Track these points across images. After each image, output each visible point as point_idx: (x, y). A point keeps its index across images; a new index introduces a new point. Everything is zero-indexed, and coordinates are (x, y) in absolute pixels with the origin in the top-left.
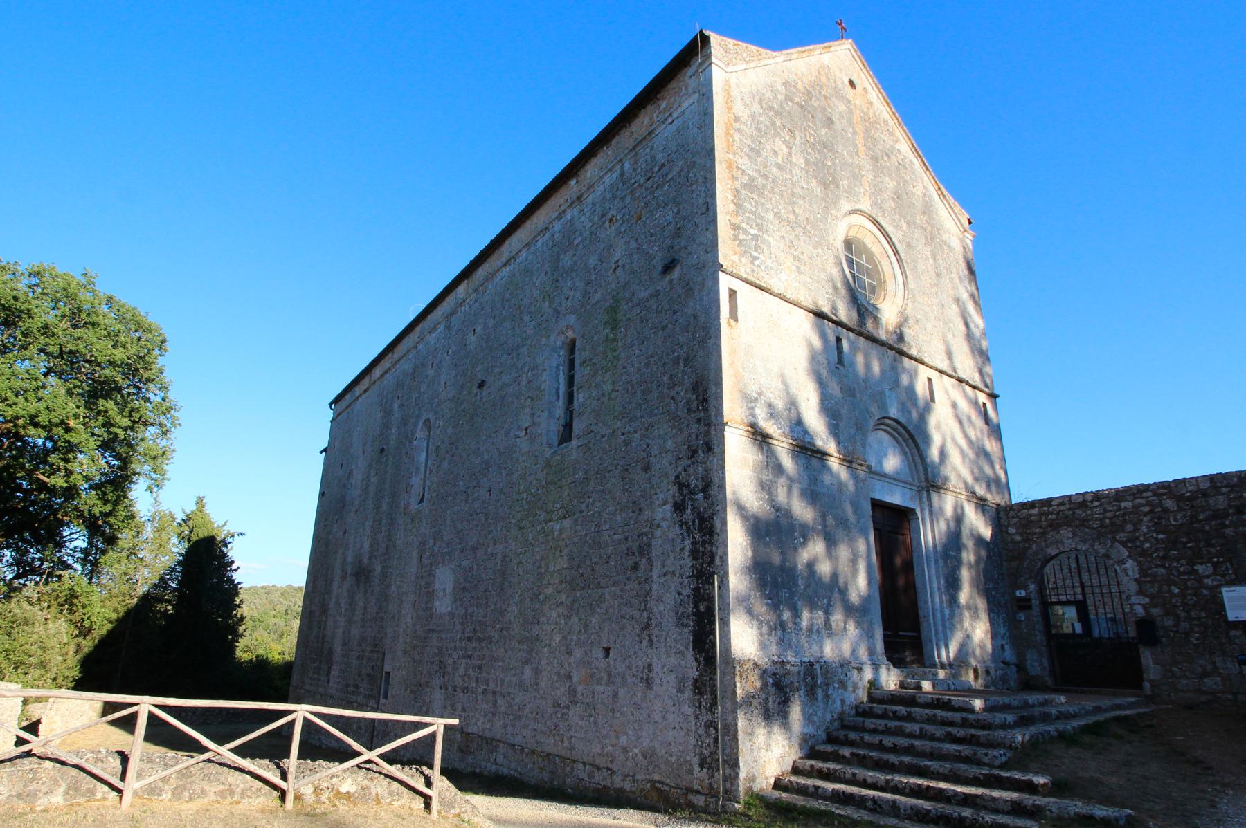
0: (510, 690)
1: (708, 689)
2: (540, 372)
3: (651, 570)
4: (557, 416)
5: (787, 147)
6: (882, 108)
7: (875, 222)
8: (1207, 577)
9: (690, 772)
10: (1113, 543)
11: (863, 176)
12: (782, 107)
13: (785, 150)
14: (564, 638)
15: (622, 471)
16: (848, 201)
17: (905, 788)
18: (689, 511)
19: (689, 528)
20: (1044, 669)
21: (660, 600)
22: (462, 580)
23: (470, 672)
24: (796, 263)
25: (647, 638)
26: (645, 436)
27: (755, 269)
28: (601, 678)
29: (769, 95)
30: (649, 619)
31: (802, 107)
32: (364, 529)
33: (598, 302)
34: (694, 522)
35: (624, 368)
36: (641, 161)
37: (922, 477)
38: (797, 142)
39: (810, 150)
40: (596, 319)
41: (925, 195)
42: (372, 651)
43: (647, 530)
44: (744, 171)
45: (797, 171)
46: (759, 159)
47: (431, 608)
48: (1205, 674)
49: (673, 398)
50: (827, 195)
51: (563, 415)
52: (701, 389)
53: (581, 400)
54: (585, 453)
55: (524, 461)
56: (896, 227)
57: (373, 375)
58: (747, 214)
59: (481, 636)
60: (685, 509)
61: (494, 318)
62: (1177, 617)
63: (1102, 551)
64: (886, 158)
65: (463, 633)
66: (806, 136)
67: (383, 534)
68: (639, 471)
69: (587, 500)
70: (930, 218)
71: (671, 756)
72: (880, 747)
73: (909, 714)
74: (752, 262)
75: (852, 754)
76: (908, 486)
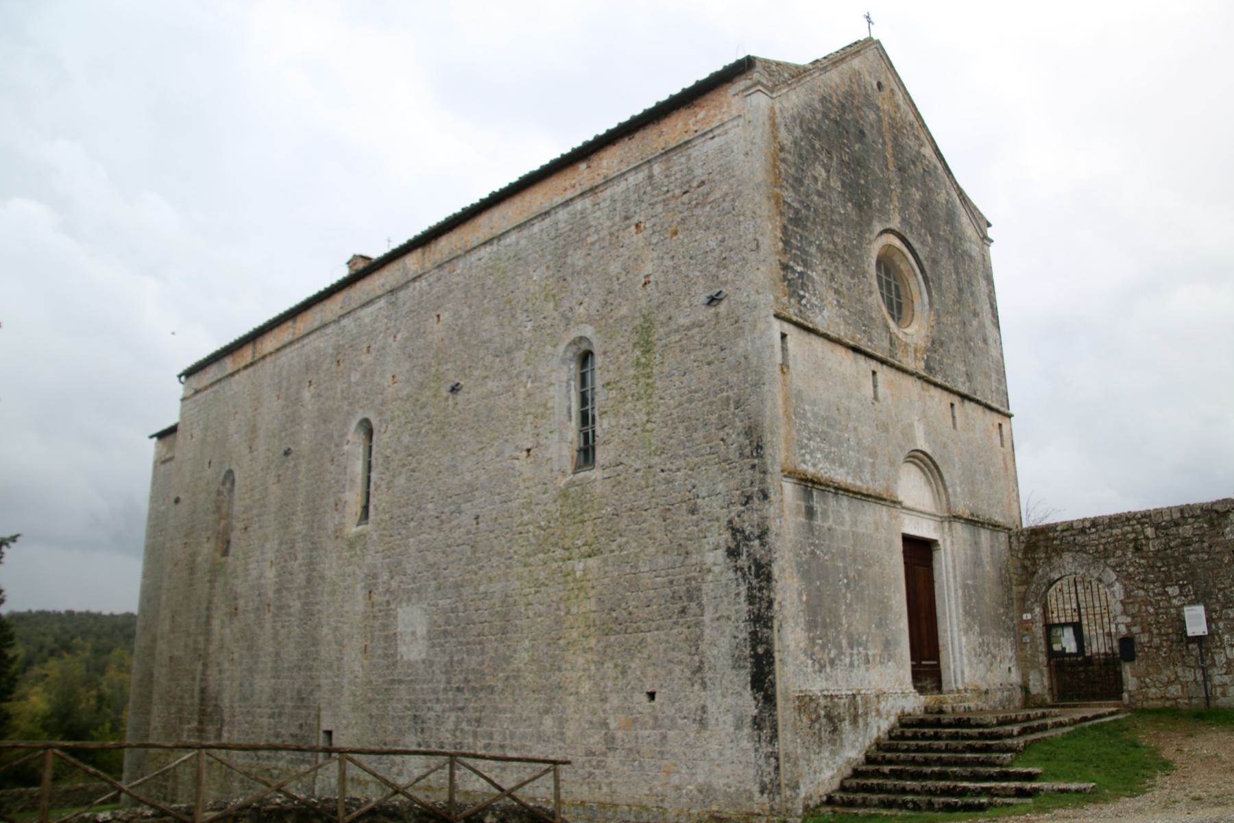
0: (524, 742)
1: (768, 724)
2: (545, 385)
3: (702, 615)
4: (570, 440)
7: (903, 240)
8: (1175, 597)
9: (750, 798)
10: (1104, 568)
11: (892, 190)
12: (820, 127)
13: (824, 174)
14: (596, 684)
15: (662, 511)
16: (880, 221)
17: (936, 790)
19: (744, 575)
20: (1044, 687)
21: (713, 644)
22: (441, 621)
23: (464, 725)
25: (700, 681)
26: (690, 476)
27: (802, 309)
28: (646, 722)
29: (808, 116)
30: (701, 662)
31: (837, 122)
32: (262, 553)
33: (624, 317)
34: (750, 568)
35: (661, 398)
37: (945, 506)
38: (834, 164)
39: (845, 170)
40: (622, 336)
41: (947, 201)
42: (295, 707)
43: (695, 574)
45: (835, 196)
46: (802, 189)
47: (394, 655)
48: (1170, 683)
49: (722, 440)
51: (576, 439)
52: (755, 436)
53: (605, 425)
54: (614, 486)
55: (527, 488)
56: (922, 243)
57: (259, 346)
58: (794, 251)
59: (477, 686)
60: (739, 554)
61: (470, 307)
62: (1151, 633)
64: (912, 167)
65: (448, 682)
67: (299, 561)
68: (685, 512)
69: (619, 539)
70: (953, 227)
71: (730, 787)
72: (913, 762)
73: (936, 733)
74: (799, 302)
75: (891, 770)
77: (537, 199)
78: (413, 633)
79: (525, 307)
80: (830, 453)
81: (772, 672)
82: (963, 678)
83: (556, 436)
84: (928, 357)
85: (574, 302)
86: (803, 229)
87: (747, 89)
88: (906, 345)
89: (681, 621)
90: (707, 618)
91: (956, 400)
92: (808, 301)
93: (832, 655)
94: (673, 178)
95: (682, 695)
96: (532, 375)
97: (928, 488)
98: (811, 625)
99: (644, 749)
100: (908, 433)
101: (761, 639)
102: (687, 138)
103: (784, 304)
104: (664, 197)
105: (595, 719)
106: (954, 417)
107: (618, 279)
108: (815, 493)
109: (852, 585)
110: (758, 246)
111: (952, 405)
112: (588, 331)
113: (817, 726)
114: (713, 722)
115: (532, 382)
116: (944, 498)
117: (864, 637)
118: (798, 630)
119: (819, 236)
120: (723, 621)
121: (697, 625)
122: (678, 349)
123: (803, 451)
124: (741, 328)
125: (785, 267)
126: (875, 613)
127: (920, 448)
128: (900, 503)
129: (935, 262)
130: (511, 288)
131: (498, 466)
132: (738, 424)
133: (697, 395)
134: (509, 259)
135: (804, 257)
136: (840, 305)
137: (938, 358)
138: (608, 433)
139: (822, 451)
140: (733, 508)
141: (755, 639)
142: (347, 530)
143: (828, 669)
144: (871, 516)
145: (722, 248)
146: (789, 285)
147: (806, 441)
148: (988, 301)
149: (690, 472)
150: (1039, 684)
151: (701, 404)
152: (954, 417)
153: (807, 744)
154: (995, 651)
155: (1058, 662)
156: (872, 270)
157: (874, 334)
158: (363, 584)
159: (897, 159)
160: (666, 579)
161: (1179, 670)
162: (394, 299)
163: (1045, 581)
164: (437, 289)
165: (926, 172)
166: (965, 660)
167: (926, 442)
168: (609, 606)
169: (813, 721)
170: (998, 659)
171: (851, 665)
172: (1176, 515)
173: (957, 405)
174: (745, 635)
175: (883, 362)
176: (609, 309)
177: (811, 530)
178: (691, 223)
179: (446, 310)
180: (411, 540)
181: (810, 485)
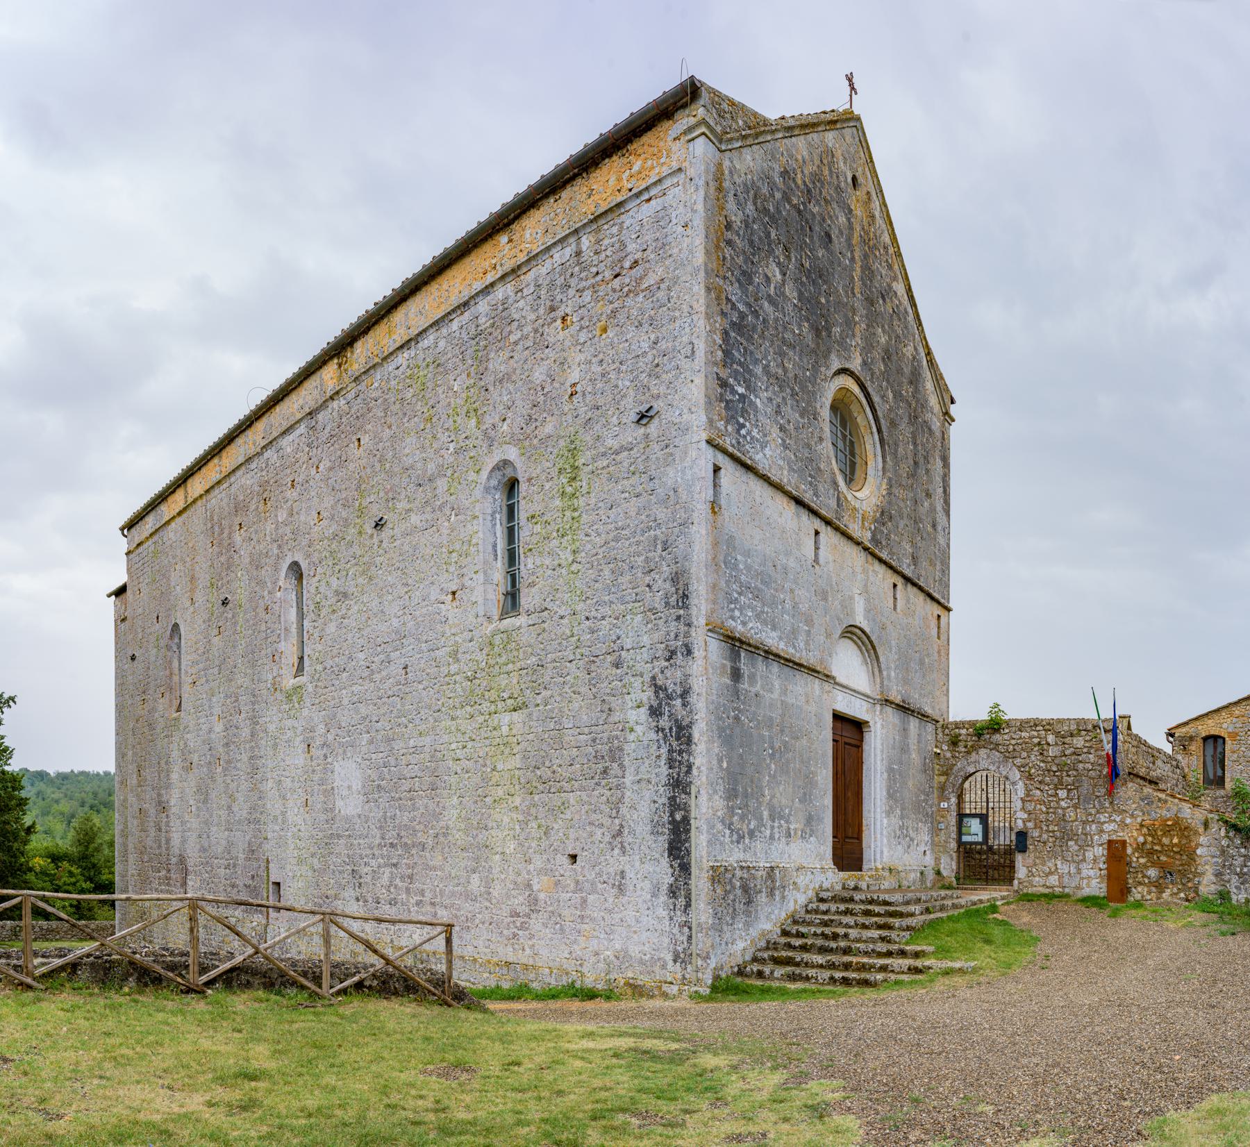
4: (495, 582)
9: (664, 967)
11: (856, 323)
13: (779, 277)
16: (839, 356)
18: (666, 718)
19: (665, 736)
21: (633, 807)
22: (374, 777)
25: (619, 846)
30: (622, 826)
31: (799, 212)
34: (671, 729)
39: (804, 279)
41: (914, 358)
45: (789, 308)
46: (751, 288)
47: (332, 810)
48: (1051, 873)
49: (648, 586)
54: (539, 635)
58: (735, 366)
61: (390, 427)
63: (1004, 773)
64: (881, 302)
70: (916, 390)
74: (738, 431)
77: (456, 285)
78: (349, 787)
79: (446, 426)
80: (763, 612)
81: (688, 840)
82: (882, 857)
83: (481, 576)
85: (497, 419)
86: (747, 340)
87: (690, 129)
88: (855, 509)
89: (603, 782)
90: (628, 780)
91: (900, 582)
92: (749, 433)
93: (752, 827)
94: (603, 256)
95: (602, 859)
96: (455, 507)
97: (864, 668)
98: (731, 794)
99: (566, 912)
100: (847, 606)
101: (679, 805)
102: (620, 198)
103: (720, 430)
104: (593, 281)
105: (519, 880)
106: (895, 598)
107: (543, 389)
108: (743, 654)
109: (777, 755)
110: (693, 352)
111: (895, 586)
112: (512, 454)
113: (731, 897)
114: (632, 888)
115: (456, 515)
116: (878, 680)
117: (787, 811)
118: (717, 797)
119: (766, 352)
120: (643, 784)
121: (618, 787)
122: (604, 477)
123: (733, 606)
124: (671, 455)
125: (724, 384)
126: (799, 787)
127: (859, 625)
128: (834, 678)
129: (893, 424)
130: (431, 402)
131: (424, 611)
132: (665, 568)
133: (623, 532)
134: (428, 366)
135: (747, 376)
136: (786, 446)
138: (533, 573)
139: (753, 609)
140: (656, 663)
141: (674, 805)
142: (284, 682)
143: (747, 841)
144: (803, 688)
145: (655, 352)
146: (727, 408)
147: (736, 596)
149: (615, 621)
150: (949, 867)
151: (628, 542)
152: (895, 598)
153: (719, 915)
154: (912, 834)
155: (966, 852)
156: (825, 413)
157: (820, 487)
158: (302, 737)
159: (864, 284)
160: (589, 736)
161: (1059, 863)
162: (314, 423)
163: (962, 773)
164: (356, 408)
166: (885, 841)
167: (865, 618)
168: (534, 763)
169: (727, 892)
170: (915, 842)
171: (772, 837)
172: (1073, 727)
173: (900, 586)
174: (664, 800)
175: (828, 523)
176: (534, 426)
177: (736, 693)
178: (621, 317)
179: (366, 433)
180: (344, 692)
181: (737, 644)
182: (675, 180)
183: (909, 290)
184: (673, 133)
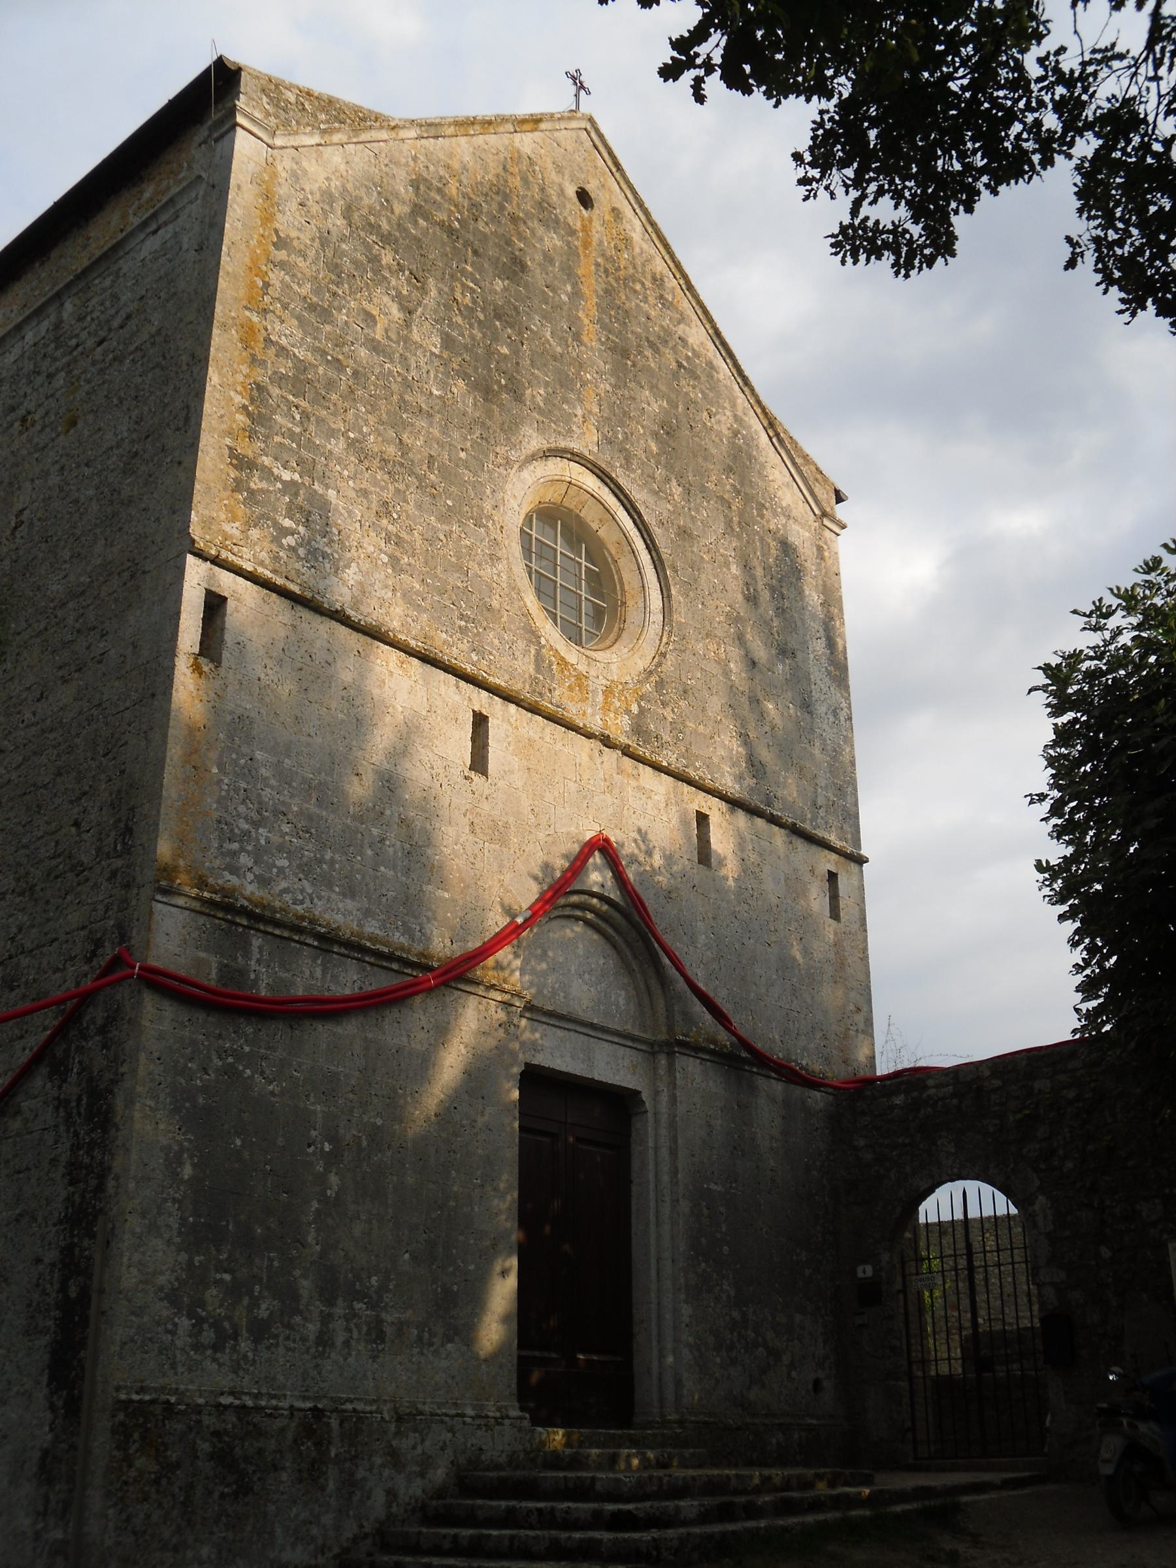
5: (402, 308)
6: (653, 251)
7: (604, 476)
16: (541, 429)
24: (390, 548)
31: (451, 231)
34: (79, 1099)
36: (94, 301)
41: (736, 434)
44: (283, 348)
50: (489, 414)
64: (648, 353)
66: (452, 289)
76: (630, 1043)
84: (642, 711)
93: (263, 1312)
108: (256, 942)
116: (661, 1004)
133: (51, 736)
137: (670, 717)
143: (244, 1346)
147: (245, 826)
148: (822, 633)
165: (688, 369)
170: (786, 1359)
171: (324, 1340)
182: (193, 195)
183: (717, 335)
184: (198, 139)
